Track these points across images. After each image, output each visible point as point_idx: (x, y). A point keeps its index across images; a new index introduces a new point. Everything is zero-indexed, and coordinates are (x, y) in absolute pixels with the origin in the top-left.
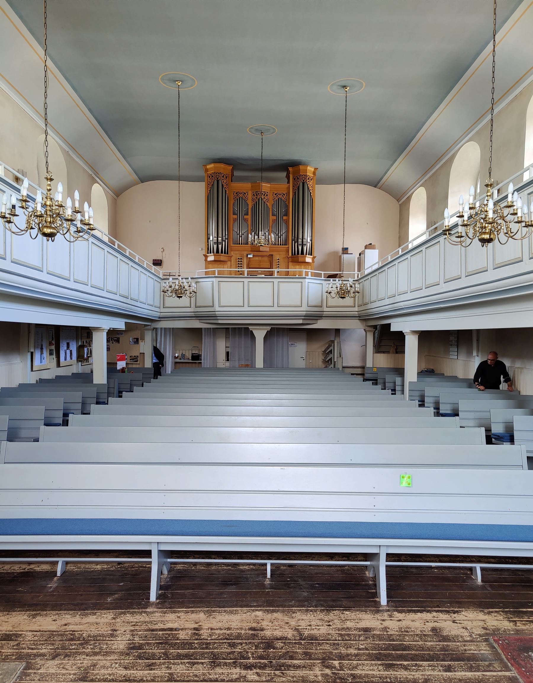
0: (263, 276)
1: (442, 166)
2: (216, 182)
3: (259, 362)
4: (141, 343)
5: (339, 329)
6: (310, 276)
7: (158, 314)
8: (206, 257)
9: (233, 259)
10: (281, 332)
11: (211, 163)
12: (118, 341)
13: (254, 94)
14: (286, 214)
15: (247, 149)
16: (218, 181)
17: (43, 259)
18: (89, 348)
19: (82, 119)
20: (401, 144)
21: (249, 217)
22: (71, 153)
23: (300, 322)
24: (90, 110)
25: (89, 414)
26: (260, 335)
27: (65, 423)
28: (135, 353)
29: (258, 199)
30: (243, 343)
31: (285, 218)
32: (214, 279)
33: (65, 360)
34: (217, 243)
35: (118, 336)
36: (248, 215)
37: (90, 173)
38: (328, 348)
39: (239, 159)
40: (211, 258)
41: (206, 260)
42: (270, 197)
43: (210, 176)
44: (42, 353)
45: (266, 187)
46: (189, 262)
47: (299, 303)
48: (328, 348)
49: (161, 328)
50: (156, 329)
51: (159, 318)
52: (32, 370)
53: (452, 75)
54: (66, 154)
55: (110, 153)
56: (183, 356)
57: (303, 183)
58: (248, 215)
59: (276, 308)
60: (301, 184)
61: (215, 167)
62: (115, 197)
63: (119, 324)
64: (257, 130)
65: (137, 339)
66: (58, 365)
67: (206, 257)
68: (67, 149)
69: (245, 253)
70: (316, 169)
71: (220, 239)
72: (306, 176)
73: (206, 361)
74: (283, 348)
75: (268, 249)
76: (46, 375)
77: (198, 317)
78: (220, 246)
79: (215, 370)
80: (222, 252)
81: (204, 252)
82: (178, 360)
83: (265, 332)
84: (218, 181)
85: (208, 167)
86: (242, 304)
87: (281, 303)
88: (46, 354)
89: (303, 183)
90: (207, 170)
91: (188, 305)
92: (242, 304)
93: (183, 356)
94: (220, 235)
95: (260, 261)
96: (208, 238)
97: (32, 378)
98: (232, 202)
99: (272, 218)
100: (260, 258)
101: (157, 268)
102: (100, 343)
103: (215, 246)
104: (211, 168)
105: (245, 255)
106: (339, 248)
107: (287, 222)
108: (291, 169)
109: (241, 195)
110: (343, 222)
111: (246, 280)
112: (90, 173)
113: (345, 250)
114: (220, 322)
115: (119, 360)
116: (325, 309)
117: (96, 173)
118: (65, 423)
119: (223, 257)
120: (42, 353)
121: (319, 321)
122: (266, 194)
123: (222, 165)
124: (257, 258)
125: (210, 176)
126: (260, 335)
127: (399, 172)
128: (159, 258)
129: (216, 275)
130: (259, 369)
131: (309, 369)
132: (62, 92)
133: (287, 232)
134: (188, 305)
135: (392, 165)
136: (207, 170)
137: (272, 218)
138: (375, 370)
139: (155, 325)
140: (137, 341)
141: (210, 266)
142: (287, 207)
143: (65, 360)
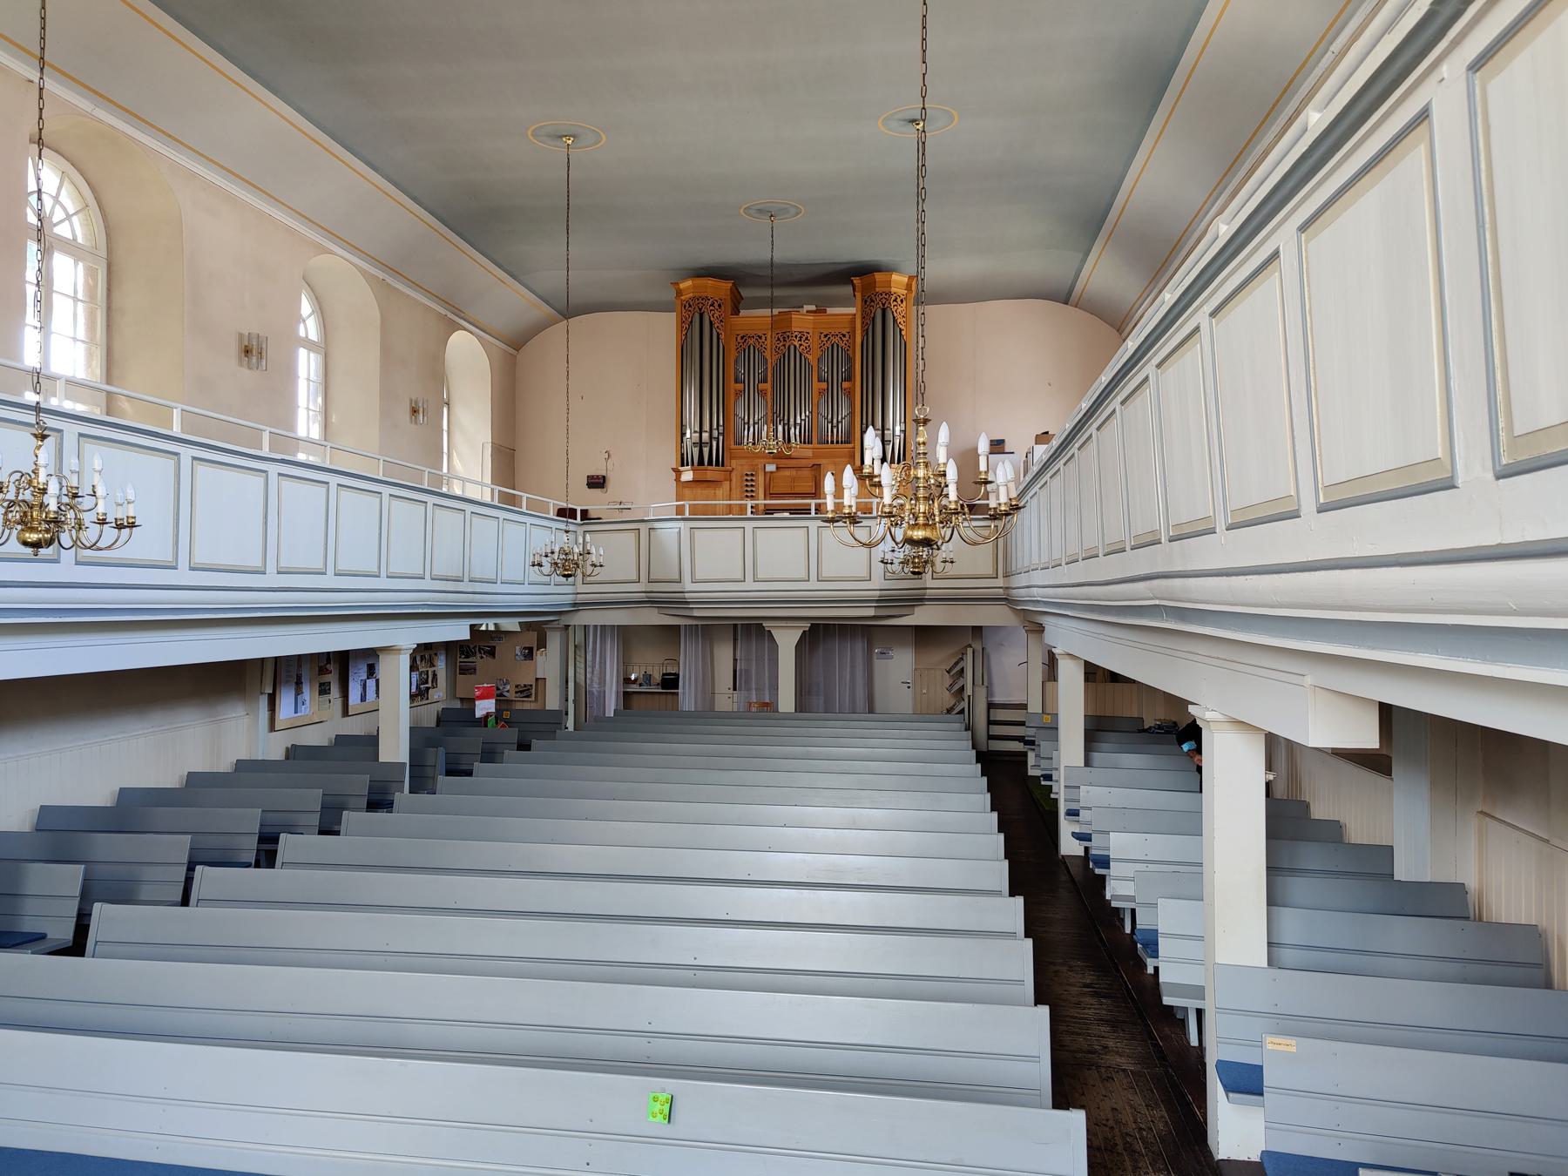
0: (786, 515)
2: (697, 316)
3: (786, 700)
4: (539, 657)
5: (980, 628)
7: (569, 599)
8: (678, 473)
10: (837, 639)
11: (684, 279)
12: (492, 653)
13: (771, 134)
14: (849, 378)
15: (749, 250)
16: (701, 315)
17: (176, 543)
18: (430, 670)
19: (402, 218)
20: (1090, 221)
21: (768, 386)
22: (390, 280)
23: (871, 612)
24: (414, 199)
25: (337, 833)
27: (267, 857)
28: (528, 680)
29: (791, 345)
31: (845, 385)
32: (681, 524)
33: (363, 698)
34: (701, 444)
35: (492, 643)
37: (443, 311)
38: (956, 663)
40: (688, 475)
41: (678, 479)
42: (814, 342)
43: (687, 306)
44: (298, 692)
45: (803, 320)
46: (649, 479)
47: (865, 574)
48: (956, 663)
49: (595, 627)
50: (567, 627)
51: (575, 605)
52: (272, 728)
53: (1147, 80)
54: (379, 286)
55: (476, 272)
56: (648, 678)
57: (884, 311)
58: (765, 381)
59: (813, 584)
60: (879, 312)
61: (694, 286)
62: (512, 351)
63: (459, 631)
64: (760, 211)
65: (531, 649)
66: (345, 713)
67: (678, 473)
68: (381, 275)
71: (705, 436)
72: (889, 294)
73: (687, 697)
74: (853, 667)
75: (809, 453)
76: (315, 737)
77: (652, 602)
78: (706, 450)
79: (707, 715)
80: (710, 463)
81: (673, 461)
82: (634, 688)
83: (797, 634)
84: (701, 315)
85: (682, 286)
86: (740, 577)
87: (825, 574)
88: (307, 693)
89: (884, 311)
90: (679, 293)
91: (635, 578)
92: (740, 577)
93: (648, 678)
94: (706, 427)
95: (794, 479)
96: (683, 434)
97: (273, 748)
98: (733, 355)
99: (817, 386)
100: (794, 472)
101: (597, 491)
102: (397, 676)
107: (850, 394)
108: (860, 276)
111: (749, 525)
112: (443, 311)
114: (696, 613)
115: (481, 697)
116: (689, 586)
117: (458, 312)
118: (267, 857)
119: (712, 473)
120: (298, 692)
121: (917, 609)
122: (802, 336)
123: (710, 282)
124: (787, 473)
125: (687, 306)
126: (787, 641)
129: (687, 515)
130: (787, 716)
131: (922, 714)
132: (345, 179)
133: (852, 414)
134: (635, 578)
135: (1084, 261)
136: (679, 293)
137: (817, 386)
139: (565, 620)
140: (529, 654)
141: (687, 492)
142: (851, 360)
143: (363, 698)
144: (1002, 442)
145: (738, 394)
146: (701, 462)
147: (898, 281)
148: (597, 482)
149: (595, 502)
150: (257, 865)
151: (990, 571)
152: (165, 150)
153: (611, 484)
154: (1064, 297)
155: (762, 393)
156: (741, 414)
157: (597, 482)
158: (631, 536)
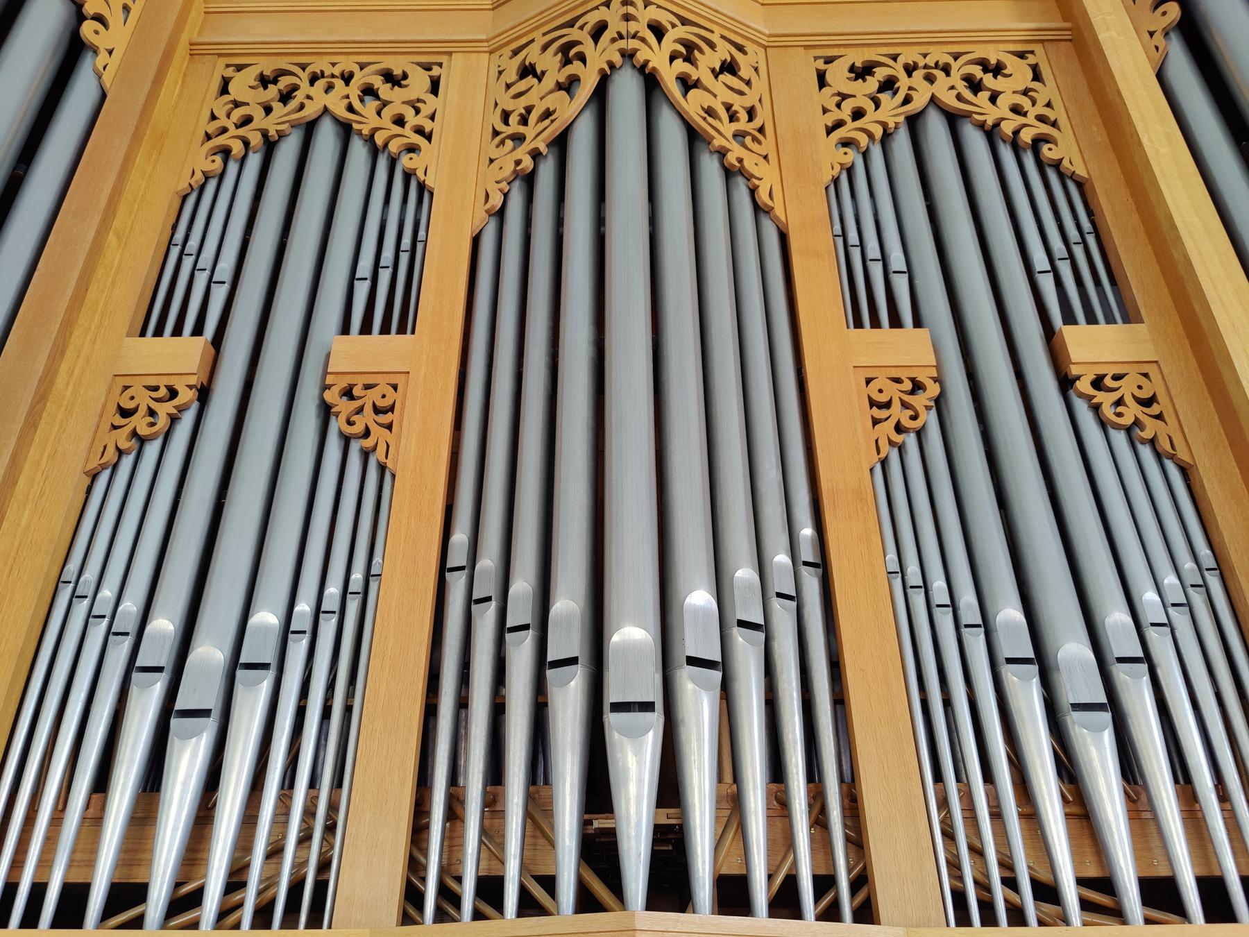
21: (419, 362)
31: (1091, 346)
36: (399, 317)
58: (399, 317)
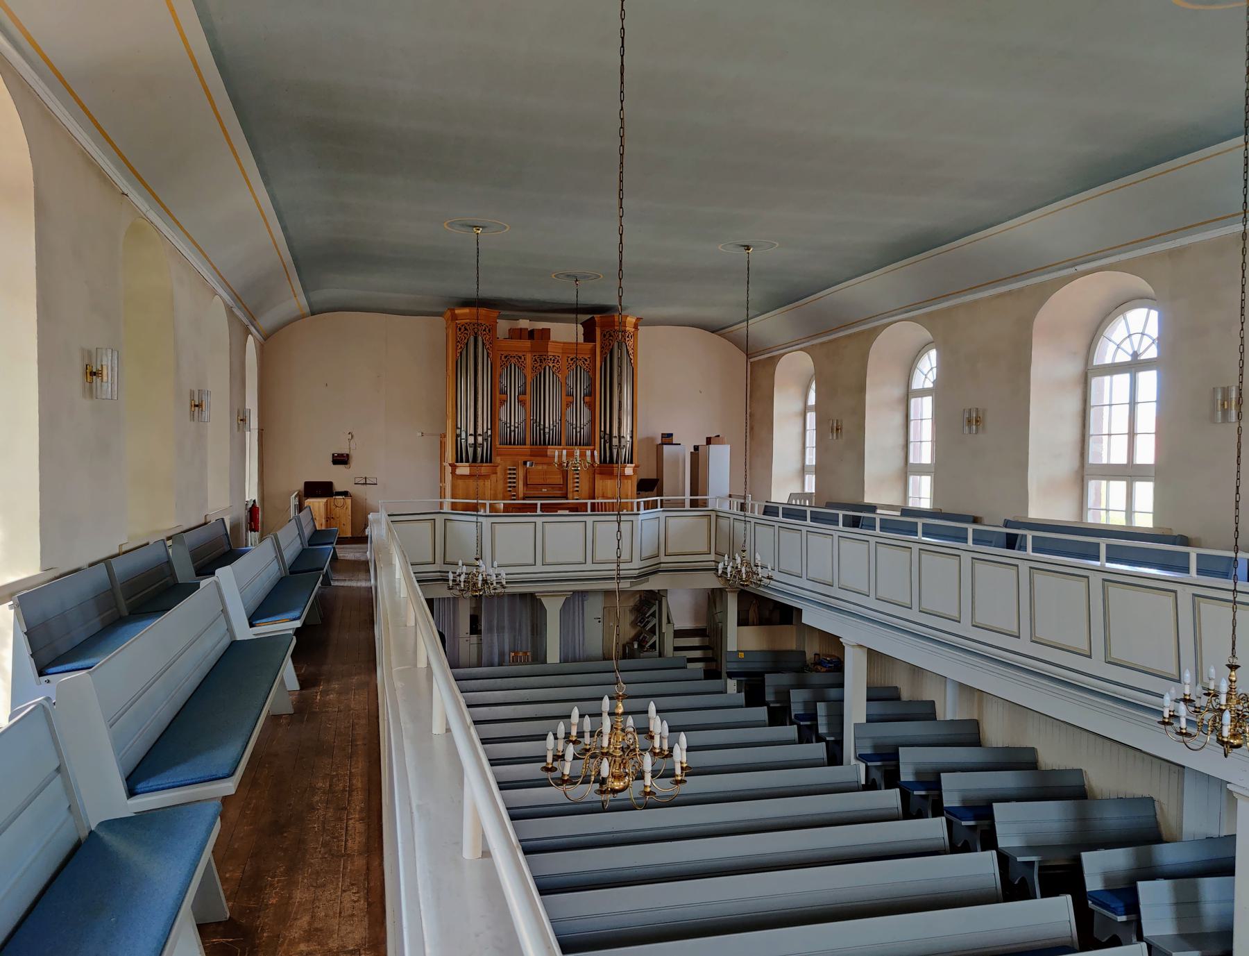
0: (567, 512)
1: (849, 336)
6: (642, 511)
9: (499, 469)
26: (553, 608)
30: (506, 605)
31: (587, 399)
34: (475, 445)
36: (525, 393)
39: (511, 300)
59: (589, 566)
67: (454, 467)
69: (521, 460)
70: (638, 319)
72: (625, 331)
78: (479, 450)
80: (482, 461)
91: (431, 560)
95: (546, 473)
101: (340, 468)
103: (471, 450)
104: (464, 314)
105: (521, 462)
106: (657, 431)
109: (513, 361)
110: (671, 394)
113: (667, 438)
116: (663, 559)
119: (485, 469)
127: (767, 326)
128: (345, 451)
133: (592, 421)
134: (431, 560)
138: (742, 655)
144: (671, 435)
145: (502, 402)
146: (475, 460)
147: (631, 320)
148: (341, 460)
149: (340, 478)
150: (801, 742)
151: (705, 549)
152: (153, 216)
153: (354, 462)
154: (715, 329)
155: (523, 403)
156: (504, 419)
157: (341, 460)
158: (428, 525)
